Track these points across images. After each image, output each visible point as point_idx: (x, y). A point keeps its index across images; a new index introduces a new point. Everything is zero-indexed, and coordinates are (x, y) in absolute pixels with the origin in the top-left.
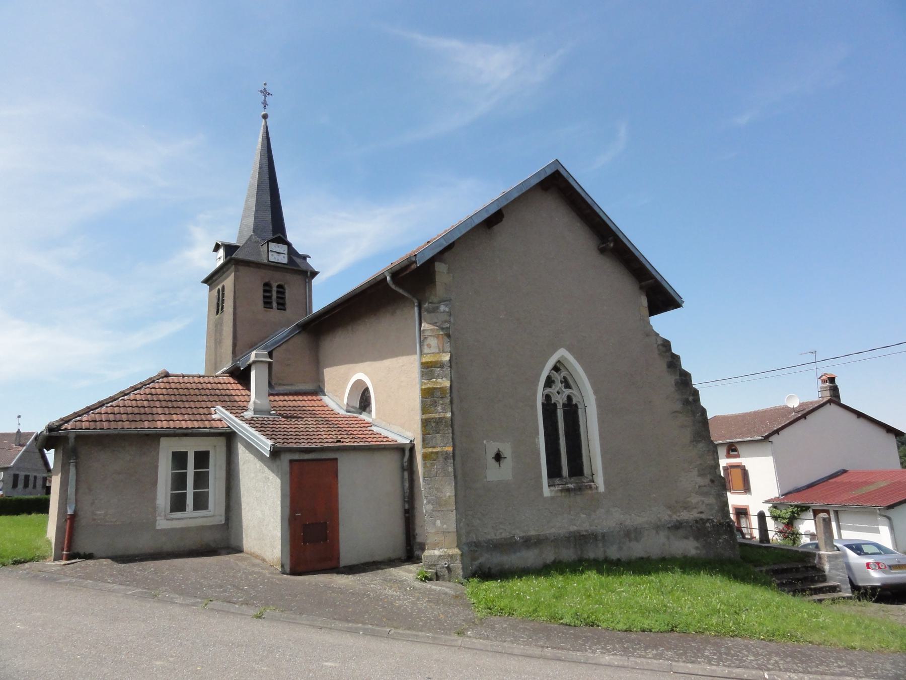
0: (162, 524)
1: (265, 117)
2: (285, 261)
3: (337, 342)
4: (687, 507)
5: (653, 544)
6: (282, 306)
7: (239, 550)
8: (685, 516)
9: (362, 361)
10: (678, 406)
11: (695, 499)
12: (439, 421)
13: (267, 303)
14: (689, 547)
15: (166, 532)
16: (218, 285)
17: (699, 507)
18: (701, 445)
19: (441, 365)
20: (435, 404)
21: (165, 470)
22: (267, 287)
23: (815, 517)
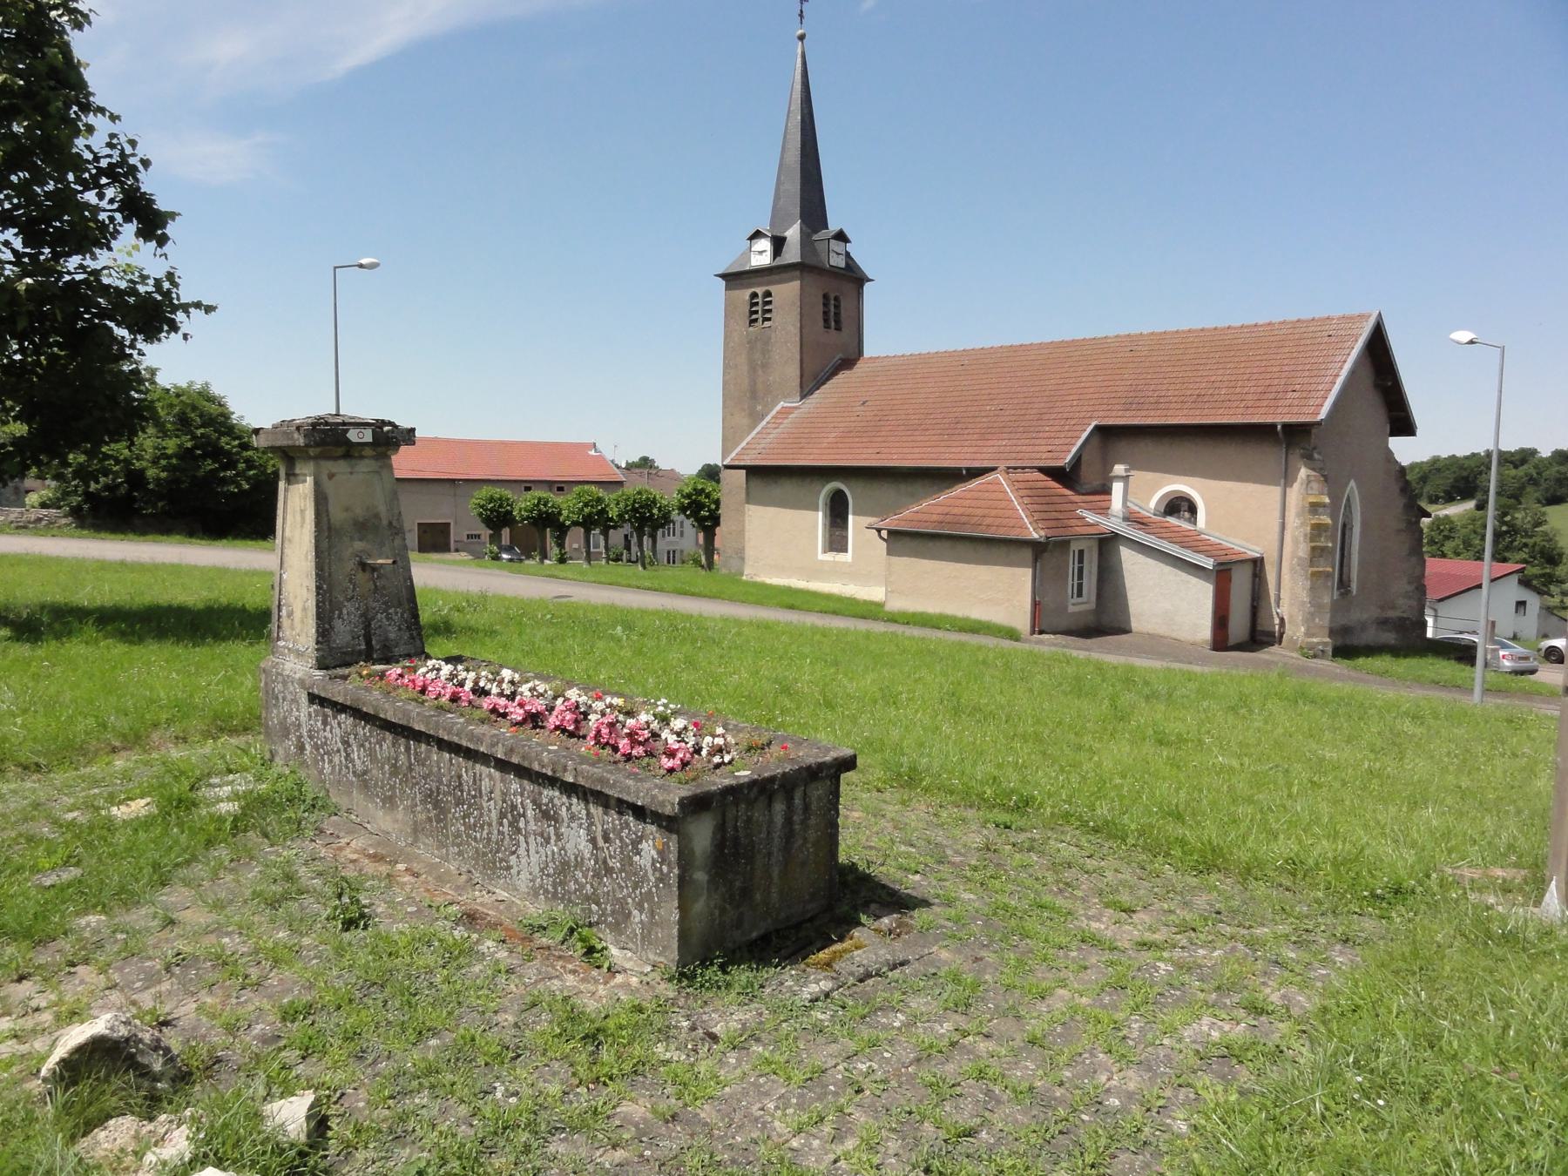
0: (1071, 609)
1: (802, 38)
2: (843, 265)
3: (1123, 446)
4: (1393, 608)
5: (1371, 636)
6: (838, 329)
7: (1127, 631)
8: (1392, 614)
9: (1192, 475)
10: (1403, 526)
11: (1401, 601)
12: (1323, 549)
13: (827, 326)
14: (1390, 638)
15: (1074, 614)
16: (759, 285)
17: (1403, 608)
18: (1414, 559)
19: (1324, 505)
20: (1320, 535)
21: (1072, 566)
22: (826, 297)
23: (1035, 560)
